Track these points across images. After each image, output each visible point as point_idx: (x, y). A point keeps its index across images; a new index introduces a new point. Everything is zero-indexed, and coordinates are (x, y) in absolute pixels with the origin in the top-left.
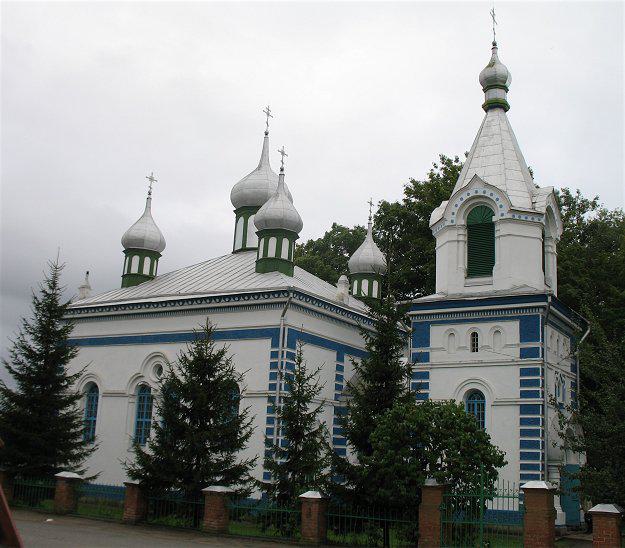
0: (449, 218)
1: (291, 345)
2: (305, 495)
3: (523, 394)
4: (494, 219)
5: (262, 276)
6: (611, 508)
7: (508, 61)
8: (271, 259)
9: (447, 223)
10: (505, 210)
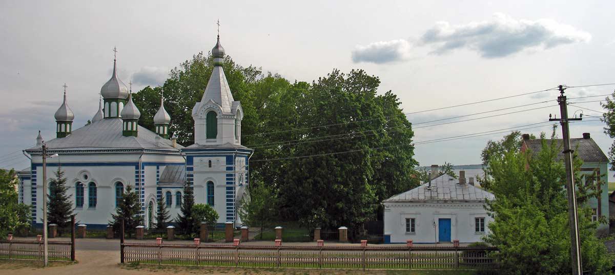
2: (277, 228)
3: (227, 183)
6: (280, 227)
8: (129, 131)
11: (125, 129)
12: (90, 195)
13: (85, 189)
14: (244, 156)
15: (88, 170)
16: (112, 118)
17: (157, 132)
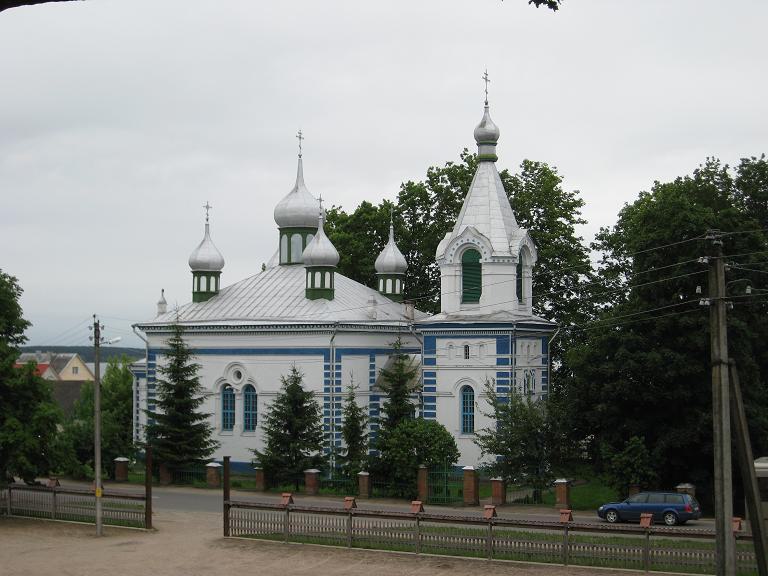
0: (449, 258)
1: (339, 359)
2: (558, 481)
4: (481, 261)
5: (312, 303)
7: (498, 122)
8: (318, 289)
9: (448, 262)
10: (488, 256)
11: (309, 286)
12: (247, 408)
13: (237, 397)
14: (492, 337)
15: (242, 362)
16: (293, 264)
17: (381, 289)
